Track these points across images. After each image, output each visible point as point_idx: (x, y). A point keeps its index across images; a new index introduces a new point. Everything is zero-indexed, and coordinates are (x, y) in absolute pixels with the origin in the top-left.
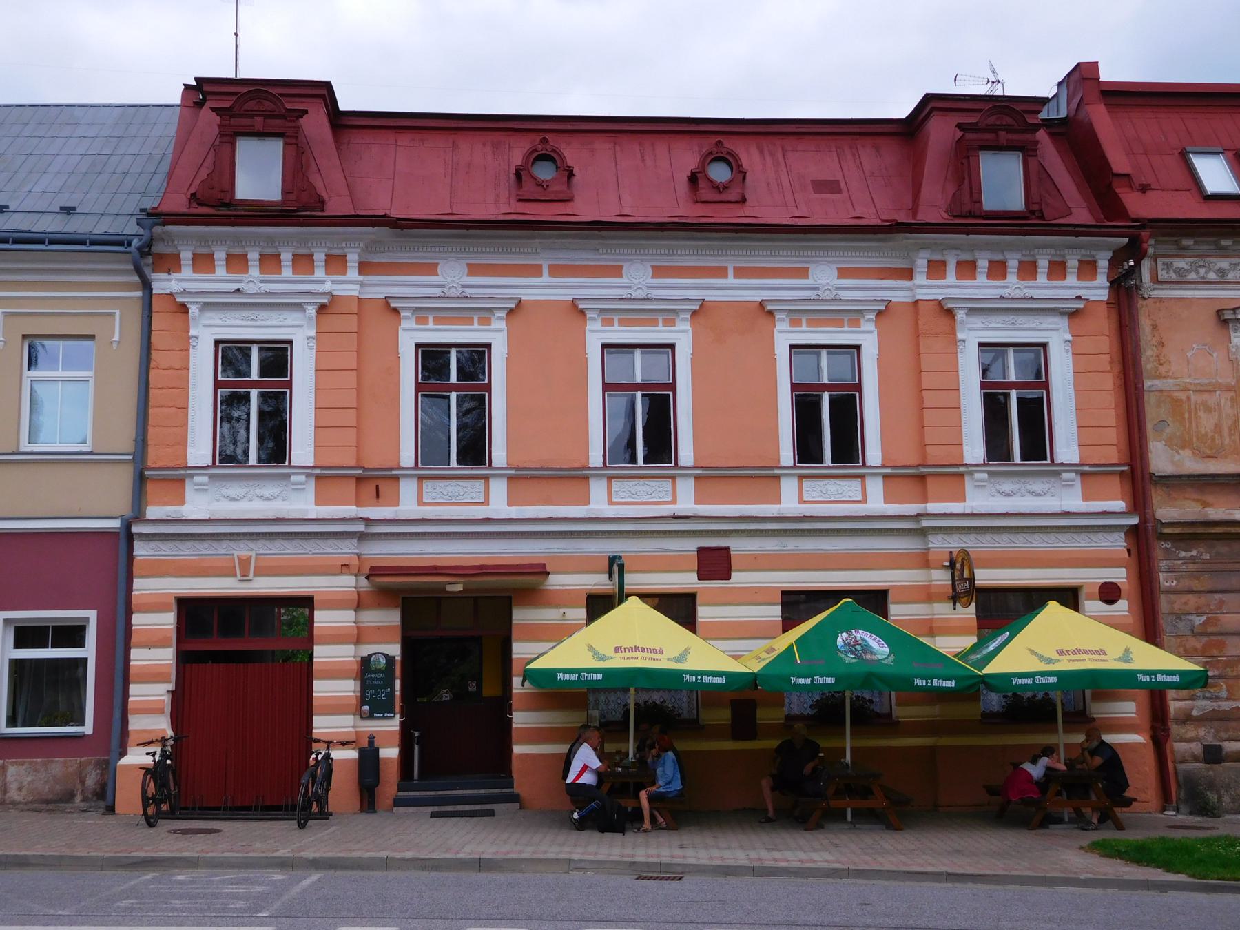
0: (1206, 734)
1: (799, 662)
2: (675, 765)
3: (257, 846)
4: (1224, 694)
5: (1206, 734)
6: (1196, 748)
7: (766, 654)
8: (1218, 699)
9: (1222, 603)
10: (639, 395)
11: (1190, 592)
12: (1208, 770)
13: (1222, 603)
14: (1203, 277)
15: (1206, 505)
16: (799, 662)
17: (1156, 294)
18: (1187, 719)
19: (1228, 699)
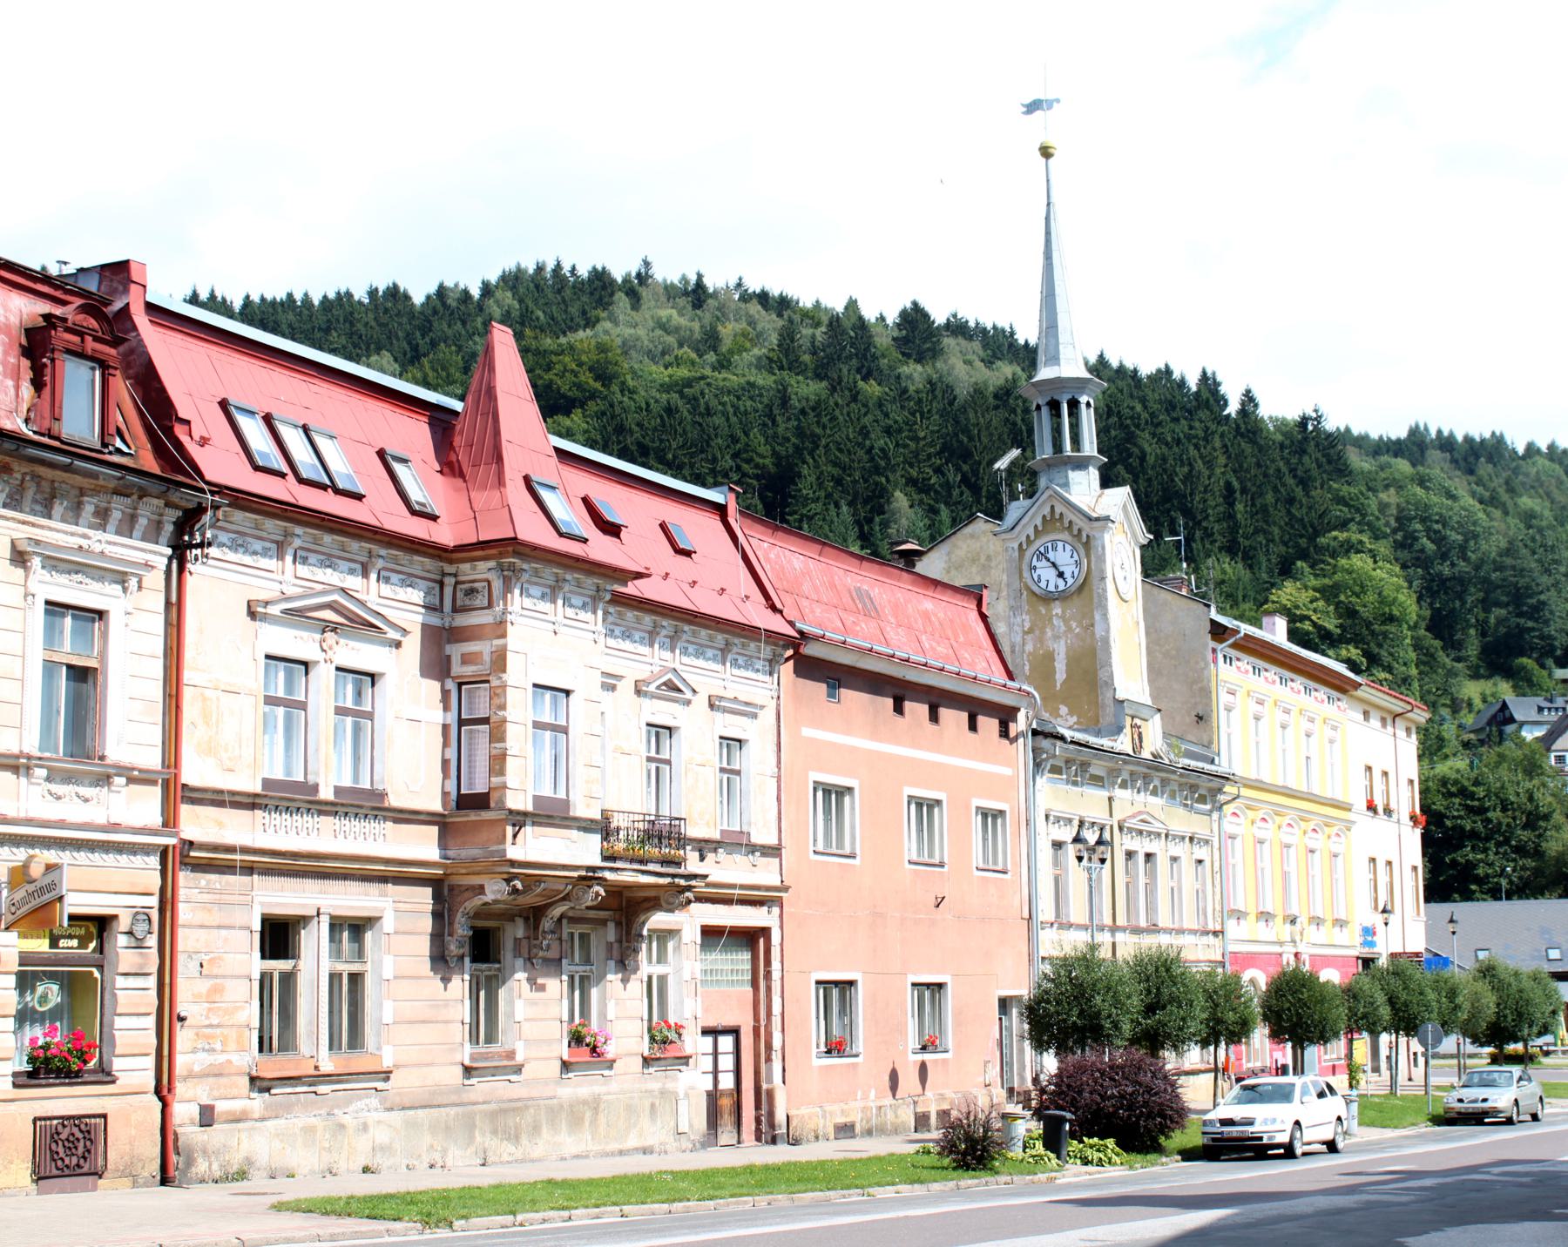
1: (807, 732)
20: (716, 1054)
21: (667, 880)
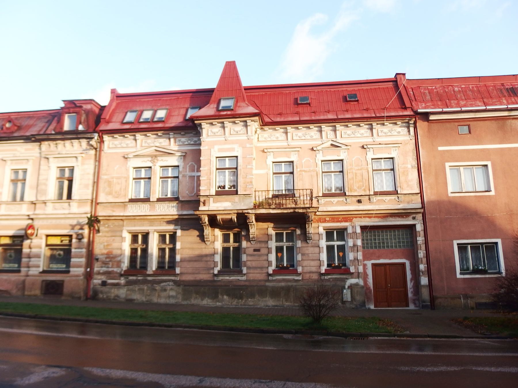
0: (104, 278)
1: (440, 148)
2: (180, 134)
3: (439, 103)
4: (110, 266)
5: (104, 278)
6: (100, 282)
7: (310, 137)
8: (108, 267)
9: (114, 240)
10: (469, 246)
11: (105, 236)
12: (101, 288)
13: (114, 240)
14: (189, 143)
15: (113, 211)
16: (440, 148)
17: (230, 139)
18: (99, 273)
19: (112, 267)
21: (292, 211)
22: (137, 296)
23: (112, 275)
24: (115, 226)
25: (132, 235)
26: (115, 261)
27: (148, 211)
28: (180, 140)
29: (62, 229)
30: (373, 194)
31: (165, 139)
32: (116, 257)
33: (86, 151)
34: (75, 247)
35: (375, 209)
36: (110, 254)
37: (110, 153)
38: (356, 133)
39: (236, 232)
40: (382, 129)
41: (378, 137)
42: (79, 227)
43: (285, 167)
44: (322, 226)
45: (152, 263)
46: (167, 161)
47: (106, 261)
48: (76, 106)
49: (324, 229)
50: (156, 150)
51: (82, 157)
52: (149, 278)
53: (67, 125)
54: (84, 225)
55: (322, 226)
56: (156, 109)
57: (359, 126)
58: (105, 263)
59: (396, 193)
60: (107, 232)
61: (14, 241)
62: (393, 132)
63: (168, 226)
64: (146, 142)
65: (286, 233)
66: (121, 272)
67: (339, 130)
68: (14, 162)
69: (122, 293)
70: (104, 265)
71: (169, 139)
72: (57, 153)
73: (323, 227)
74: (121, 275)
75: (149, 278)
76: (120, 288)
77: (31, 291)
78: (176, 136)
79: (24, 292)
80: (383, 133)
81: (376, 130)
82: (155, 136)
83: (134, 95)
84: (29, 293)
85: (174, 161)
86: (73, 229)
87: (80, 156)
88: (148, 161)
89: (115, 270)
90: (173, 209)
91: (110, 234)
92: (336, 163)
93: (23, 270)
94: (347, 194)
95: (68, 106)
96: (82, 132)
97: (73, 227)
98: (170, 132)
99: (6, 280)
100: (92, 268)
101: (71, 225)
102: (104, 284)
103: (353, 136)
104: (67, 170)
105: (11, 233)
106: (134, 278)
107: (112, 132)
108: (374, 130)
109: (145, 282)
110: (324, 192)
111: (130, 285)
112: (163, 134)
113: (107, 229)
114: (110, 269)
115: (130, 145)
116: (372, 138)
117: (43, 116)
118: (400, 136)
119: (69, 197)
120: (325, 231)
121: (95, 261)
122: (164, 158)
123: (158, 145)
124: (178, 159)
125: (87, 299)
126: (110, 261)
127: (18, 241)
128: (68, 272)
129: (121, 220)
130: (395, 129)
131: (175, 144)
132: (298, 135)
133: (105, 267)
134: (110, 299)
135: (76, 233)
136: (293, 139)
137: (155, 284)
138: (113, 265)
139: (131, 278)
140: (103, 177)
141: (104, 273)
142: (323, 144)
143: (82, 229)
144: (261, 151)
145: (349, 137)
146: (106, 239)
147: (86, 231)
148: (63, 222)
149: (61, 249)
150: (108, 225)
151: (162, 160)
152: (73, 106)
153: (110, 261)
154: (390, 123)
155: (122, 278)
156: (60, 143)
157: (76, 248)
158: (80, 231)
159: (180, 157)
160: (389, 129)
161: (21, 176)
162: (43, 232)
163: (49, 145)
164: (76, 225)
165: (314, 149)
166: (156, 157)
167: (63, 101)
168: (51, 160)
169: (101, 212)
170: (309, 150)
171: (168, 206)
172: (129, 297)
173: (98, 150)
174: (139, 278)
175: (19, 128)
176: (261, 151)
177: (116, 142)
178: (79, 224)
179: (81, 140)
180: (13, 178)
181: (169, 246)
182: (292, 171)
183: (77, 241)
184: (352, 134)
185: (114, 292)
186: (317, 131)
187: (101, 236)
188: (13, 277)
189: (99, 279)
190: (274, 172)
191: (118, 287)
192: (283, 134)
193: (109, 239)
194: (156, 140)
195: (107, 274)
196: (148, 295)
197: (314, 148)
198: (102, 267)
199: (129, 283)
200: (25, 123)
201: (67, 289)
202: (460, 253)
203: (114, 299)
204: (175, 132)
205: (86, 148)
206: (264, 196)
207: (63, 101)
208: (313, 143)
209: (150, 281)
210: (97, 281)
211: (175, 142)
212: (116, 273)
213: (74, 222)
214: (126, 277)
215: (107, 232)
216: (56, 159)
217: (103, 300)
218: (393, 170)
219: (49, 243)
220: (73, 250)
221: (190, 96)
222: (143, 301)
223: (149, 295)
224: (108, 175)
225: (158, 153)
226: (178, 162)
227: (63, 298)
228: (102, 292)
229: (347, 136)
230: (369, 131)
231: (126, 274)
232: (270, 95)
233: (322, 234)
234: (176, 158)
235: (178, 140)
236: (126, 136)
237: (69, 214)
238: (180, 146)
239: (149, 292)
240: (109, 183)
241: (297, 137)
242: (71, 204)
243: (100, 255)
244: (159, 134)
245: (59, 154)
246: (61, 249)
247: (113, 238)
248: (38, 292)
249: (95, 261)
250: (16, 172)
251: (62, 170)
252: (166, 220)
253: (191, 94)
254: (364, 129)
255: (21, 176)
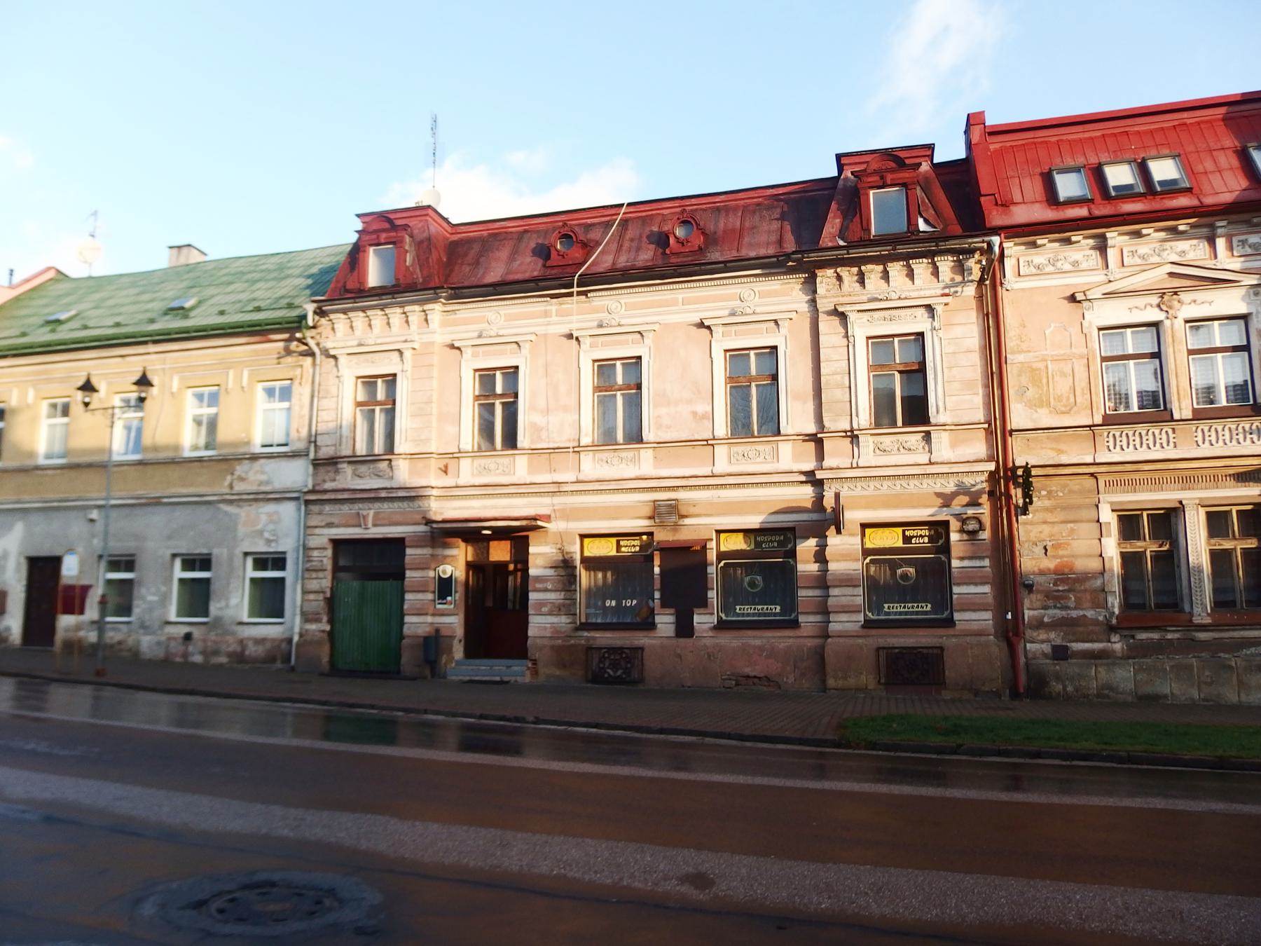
0: (1055, 637)
4: (1072, 604)
5: (1055, 637)
6: (1046, 648)
8: (1066, 608)
9: (1072, 530)
11: (1045, 522)
15: (1060, 452)
18: (1039, 624)
19: (1076, 608)
20: (634, 546)
22: (1169, 687)
23: (1081, 629)
24: (1071, 492)
25: (1118, 516)
26: (1085, 591)
27: (1169, 448)
28: (1243, 242)
29: (914, 507)
30: (1191, 417)
31: (1195, 242)
32: (1085, 577)
33: (953, 290)
34: (961, 555)
35: (570, 481)
36: (1066, 571)
37: (1023, 290)
38: (1167, 252)
39: (1162, 512)
40: (1029, 258)
41: (1018, 279)
42: (965, 499)
43: (1220, 329)
44: (1109, 502)
45: (1202, 591)
46: (1210, 303)
47: (1058, 591)
48: (394, 227)
49: (1113, 511)
50: (1171, 274)
51: (414, 349)
52: (1202, 636)
53: (374, 274)
54: (980, 492)
55: (1109, 502)
56: (1093, 160)
57: (1068, 241)
58: (1053, 598)
59: (1169, 418)
60: (1049, 510)
61: (758, 544)
62: (1060, 263)
63: (1242, 486)
64: (1133, 253)
65: (1237, 511)
66: (1108, 621)
67: (1114, 247)
68: (481, 349)
69: (1124, 677)
70: (1050, 603)
71: (1212, 241)
72: (865, 298)
73: (1112, 503)
74: (1112, 629)
75: (1202, 636)
76: (1114, 664)
77: (845, 678)
78: (1233, 229)
79: (824, 681)
80: (1136, 258)
81: (1014, 261)
82: (1162, 235)
83: (1078, 120)
84: (841, 683)
85: (1231, 301)
86: (946, 505)
87: (407, 348)
88: (1148, 307)
89: (1090, 614)
90: (1252, 438)
91: (1059, 516)
92: (1138, 332)
93: (808, 621)
94: (1176, 416)
95: (375, 227)
96: (929, 238)
97: (947, 500)
98: (1215, 218)
99: (761, 649)
100: (1018, 614)
101: (938, 495)
102: (1060, 653)
103: (1050, 269)
104: (499, 376)
105: (754, 521)
106: (1155, 636)
107: (1028, 232)
108: (1110, 252)
109: (1190, 646)
110: (1195, 406)
111: (1144, 656)
112: (1193, 226)
113: (1047, 503)
114: (1074, 614)
115: (1084, 266)
116: (1105, 272)
117: (758, 204)
118: (1042, 277)
119: (511, 440)
120: (1115, 514)
121: (1023, 592)
122: (1201, 296)
123: (1175, 258)
124: (1248, 294)
125: (1015, 694)
126: (1069, 591)
127: (770, 543)
128: (950, 622)
129: (1092, 475)
130: (1066, 254)
131: (1230, 254)
132: (1034, 263)
133: (1055, 607)
134: (1086, 696)
135: (957, 516)
136: (1021, 274)
137: (1221, 652)
138: (1078, 601)
139: (1143, 636)
140: (1015, 360)
141: (1055, 625)
142: (1110, 281)
143: (974, 503)
144: (1065, 298)
145: (1040, 272)
146: (1047, 529)
147: (985, 511)
148: (913, 485)
149: (909, 563)
150: (1050, 492)
151: (1195, 301)
152: (387, 226)
153: (1069, 591)
154: (1051, 241)
155: (1115, 638)
156: (872, 271)
157: (962, 559)
158: (971, 511)
159: (1251, 291)
160: (1049, 256)
161: (381, 394)
162: (853, 516)
163: (839, 278)
164: (954, 495)
165: (1078, 299)
166: (1176, 293)
167: (358, 216)
168: (343, 360)
169: (1021, 455)
170: (1062, 300)
171: (1234, 432)
172: (1148, 690)
173: (991, 280)
174: (1169, 636)
175: (711, 240)
176: (1065, 298)
177: (1039, 257)
178: (962, 490)
179: (351, 314)
180: (361, 398)
181: (1247, 544)
182: (1157, 350)
183: (965, 537)
184: (1046, 265)
185: (1099, 676)
186: (1093, 248)
187: (1032, 523)
188: (781, 640)
189: (1042, 642)
190: (1190, 347)
191: (1104, 661)
192: (1092, 252)
193: (1056, 528)
194: (1168, 245)
195: (1067, 625)
196: (1205, 683)
197: (1076, 295)
198: (1045, 608)
199: (1137, 652)
200: (720, 224)
201: (953, 670)
202: (961, 573)
203: (1098, 696)
204: (1234, 217)
205: (952, 279)
206: (1186, 408)
207: (358, 216)
208: (1075, 282)
209: (1205, 645)
210: (1037, 646)
211: (1231, 248)
212: (1096, 622)
213: (950, 486)
214: (1126, 633)
215: (1049, 510)
216: (866, 316)
217: (1067, 699)
218: (1157, 355)
219: (869, 545)
220: (955, 563)
221: (1221, 116)
222: (1193, 699)
223: (1211, 684)
224: (1029, 351)
225: (1177, 283)
226: (1248, 304)
227: (947, 694)
228: (1058, 678)
229: (1034, 271)
230: (1095, 255)
231: (1123, 626)
232: (1001, 152)
233: (1110, 523)
234: (1241, 292)
235: (1239, 241)
236: (1039, 242)
237: (578, 482)
238: (1248, 258)
239: (1207, 673)
240: (1035, 375)
241: (1032, 267)
242: (393, 463)
243: (1034, 573)
244: (1181, 228)
245: (360, 345)
246: (909, 563)
247: (1070, 525)
248: (867, 679)
249: (1023, 592)
250: (369, 382)
251: (486, 377)
252: (1232, 471)
253: (1223, 110)
254: (1082, 250)
255: (381, 394)
